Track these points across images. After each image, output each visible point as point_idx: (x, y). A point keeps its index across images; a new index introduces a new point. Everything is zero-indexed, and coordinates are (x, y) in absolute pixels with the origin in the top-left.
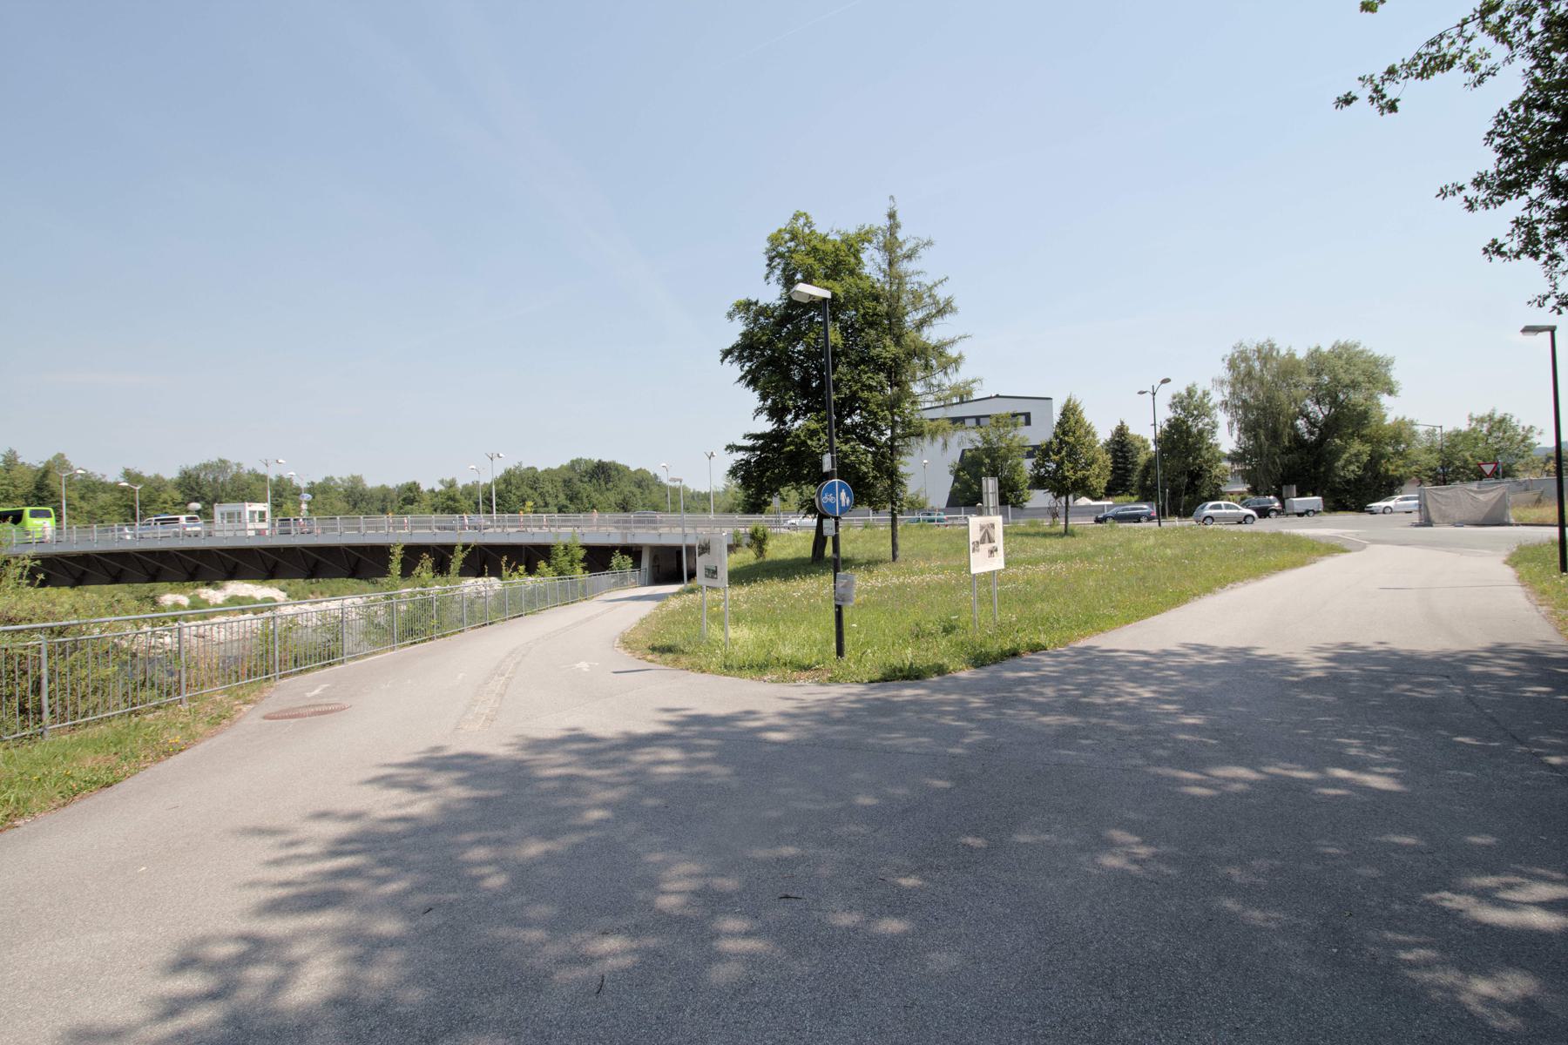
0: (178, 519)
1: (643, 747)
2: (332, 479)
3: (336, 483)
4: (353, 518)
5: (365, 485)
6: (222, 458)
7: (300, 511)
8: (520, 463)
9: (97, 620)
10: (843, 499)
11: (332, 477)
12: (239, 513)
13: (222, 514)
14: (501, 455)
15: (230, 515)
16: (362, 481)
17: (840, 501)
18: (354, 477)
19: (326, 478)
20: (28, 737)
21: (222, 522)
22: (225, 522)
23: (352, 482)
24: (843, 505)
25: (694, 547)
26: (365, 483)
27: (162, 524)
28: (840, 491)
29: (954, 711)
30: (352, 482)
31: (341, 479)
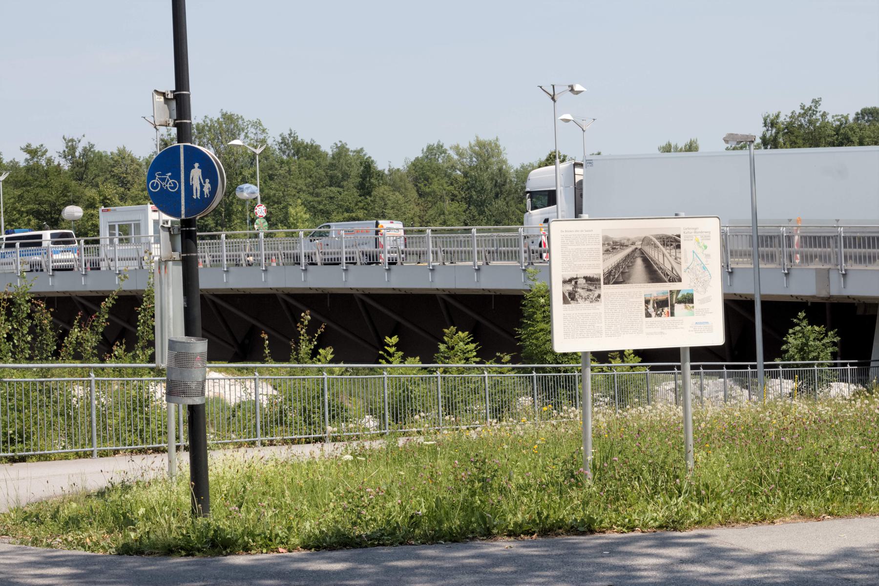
0: (40, 237)
1: (264, 579)
2: (440, 150)
3: (449, 158)
4: (451, 231)
5: (504, 162)
6: (230, 110)
7: (253, 221)
8: (816, 102)
9: (439, 383)
10: (196, 184)
11: (440, 147)
12: (138, 226)
13: (112, 227)
14: (577, 88)
15: (125, 229)
16: (499, 153)
17: (189, 188)
18: (481, 145)
19: (430, 149)
20: (349, 510)
21: (111, 241)
22: (116, 241)
23: (478, 155)
24: (196, 195)
25: (605, 283)
26: (504, 156)
27: (22, 245)
28: (189, 168)
29: (261, 578)
30: (478, 155)
31: (457, 149)
